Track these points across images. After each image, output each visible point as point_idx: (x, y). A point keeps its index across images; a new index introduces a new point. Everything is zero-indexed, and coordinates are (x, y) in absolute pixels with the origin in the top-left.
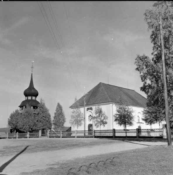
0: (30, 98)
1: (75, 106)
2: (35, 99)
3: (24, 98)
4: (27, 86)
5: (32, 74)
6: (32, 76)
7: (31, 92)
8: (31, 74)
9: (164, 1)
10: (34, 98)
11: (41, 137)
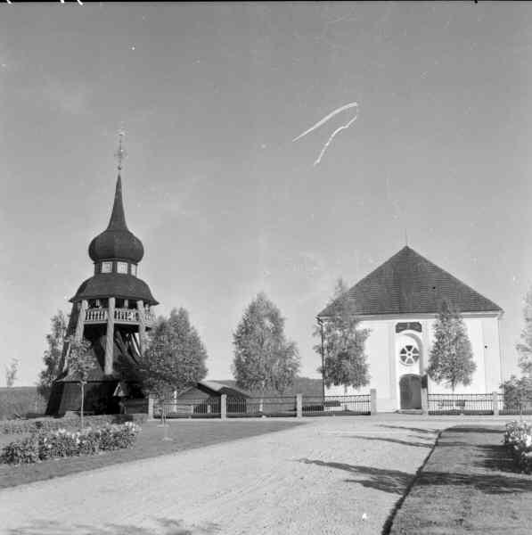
0: (106, 267)
1: (336, 314)
2: (129, 270)
3: (87, 270)
4: (100, 226)
5: (119, 178)
6: (119, 185)
7: (114, 246)
8: (116, 179)
9: (409, 496)
10: (122, 268)
11: (69, 455)
